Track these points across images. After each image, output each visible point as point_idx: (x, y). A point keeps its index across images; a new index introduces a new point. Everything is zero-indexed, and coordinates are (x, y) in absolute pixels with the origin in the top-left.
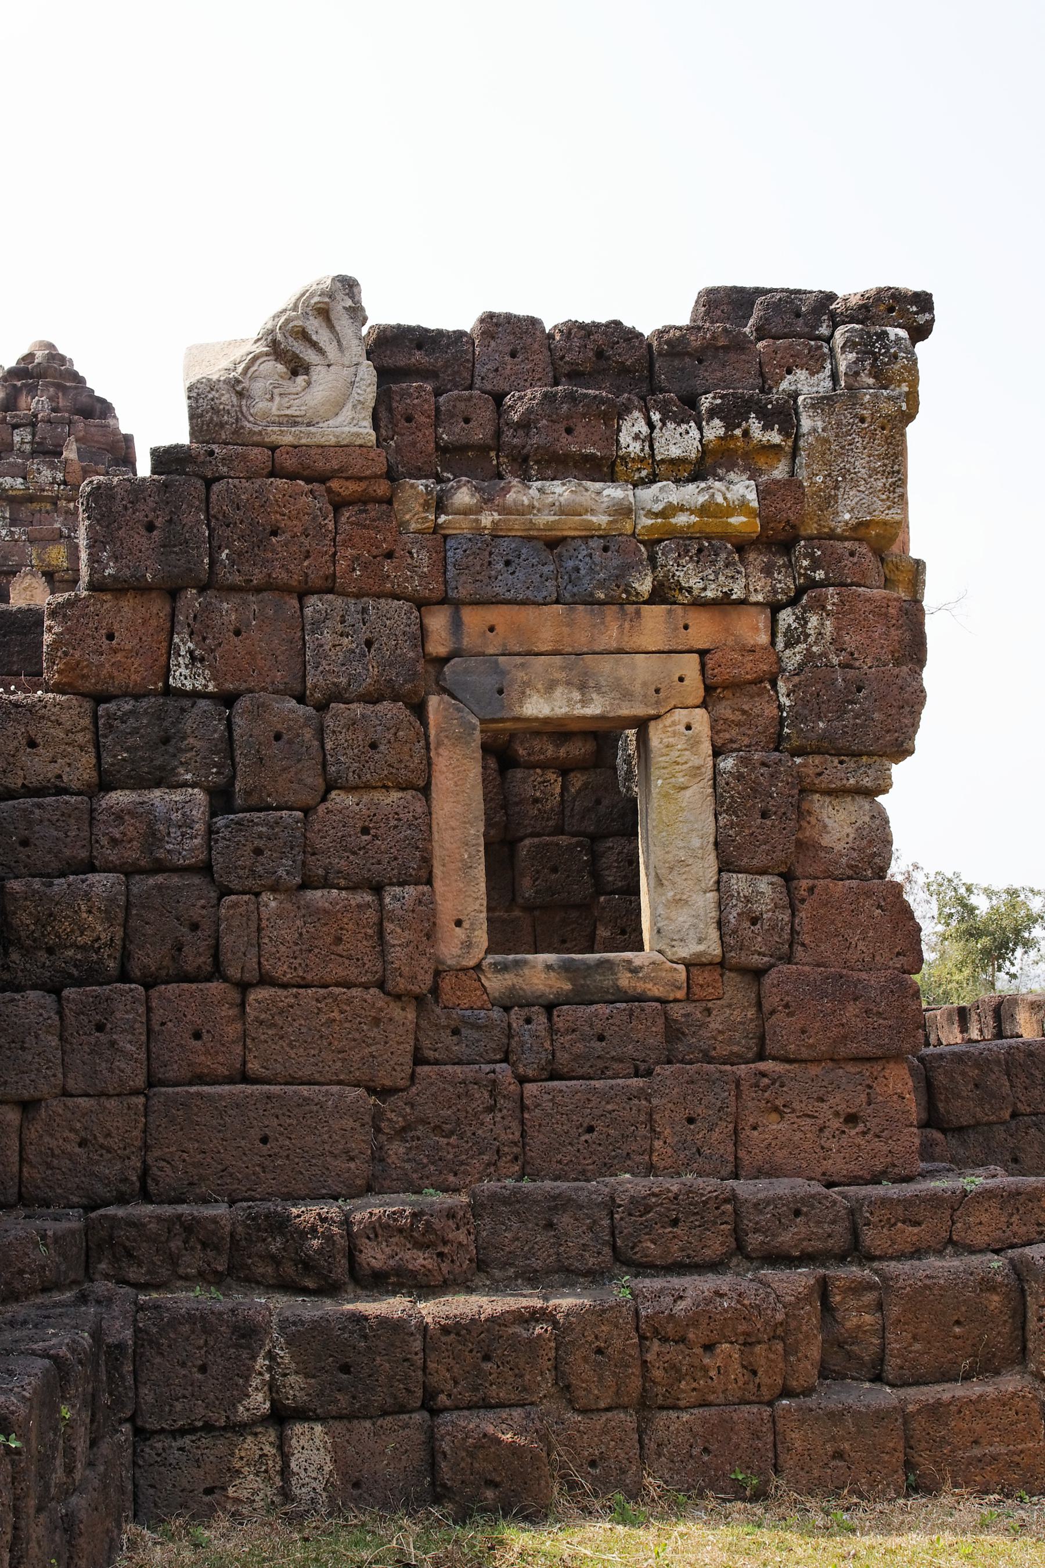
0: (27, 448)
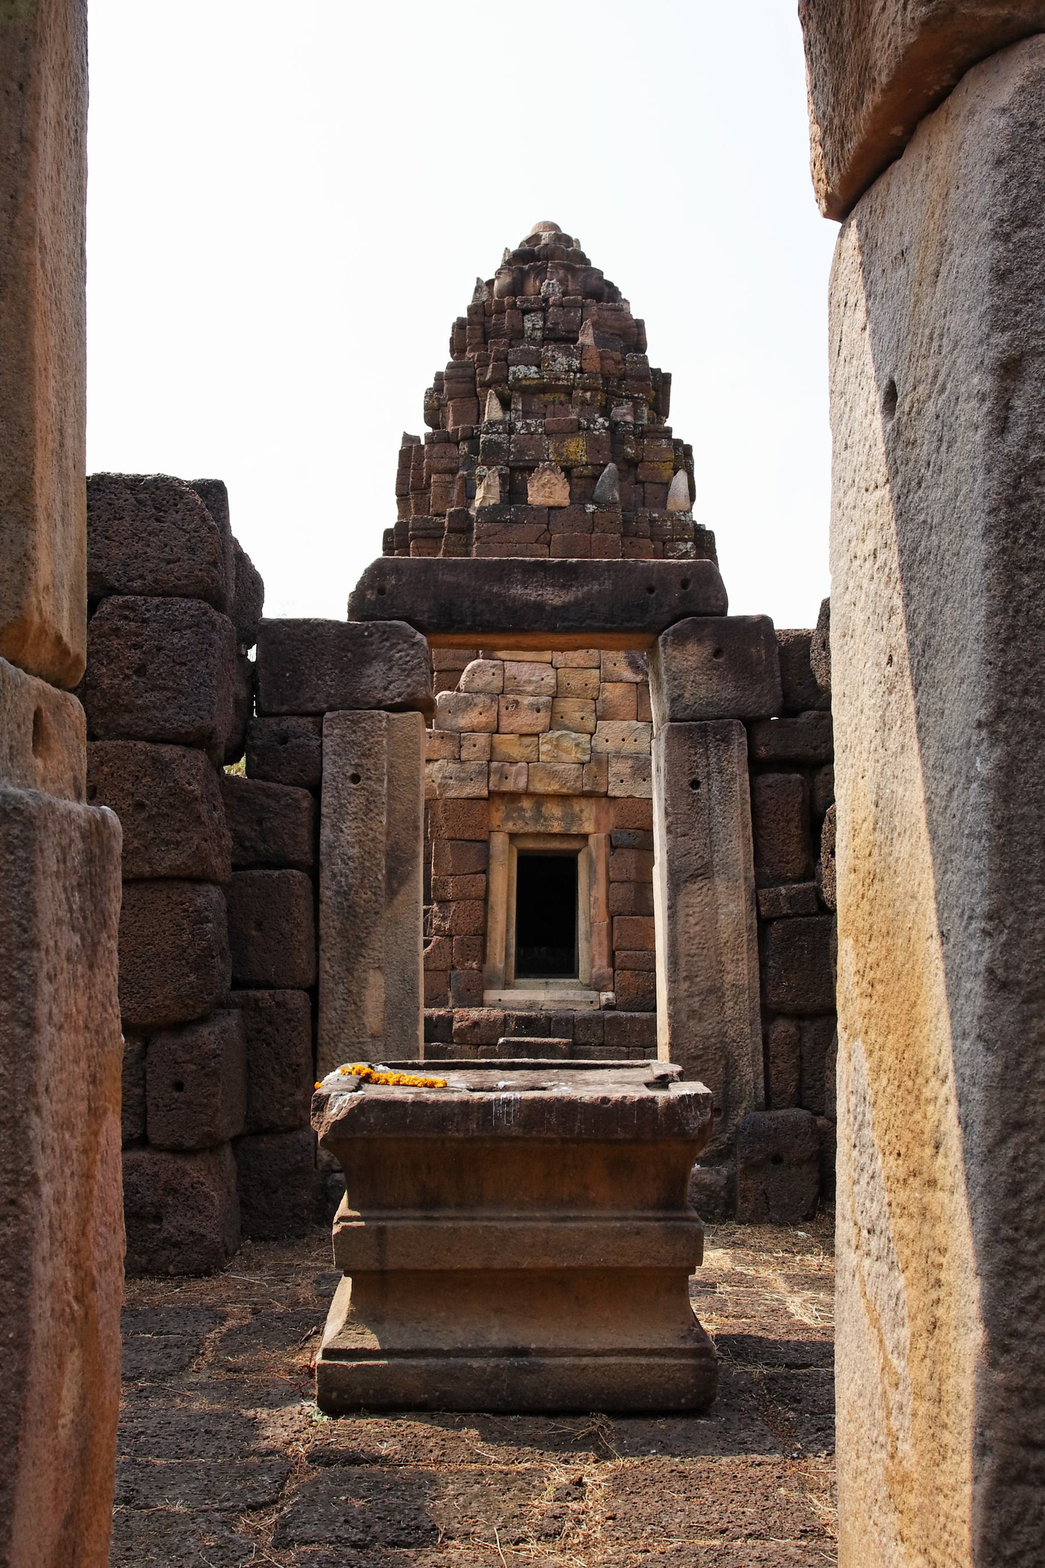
0: (539, 334)
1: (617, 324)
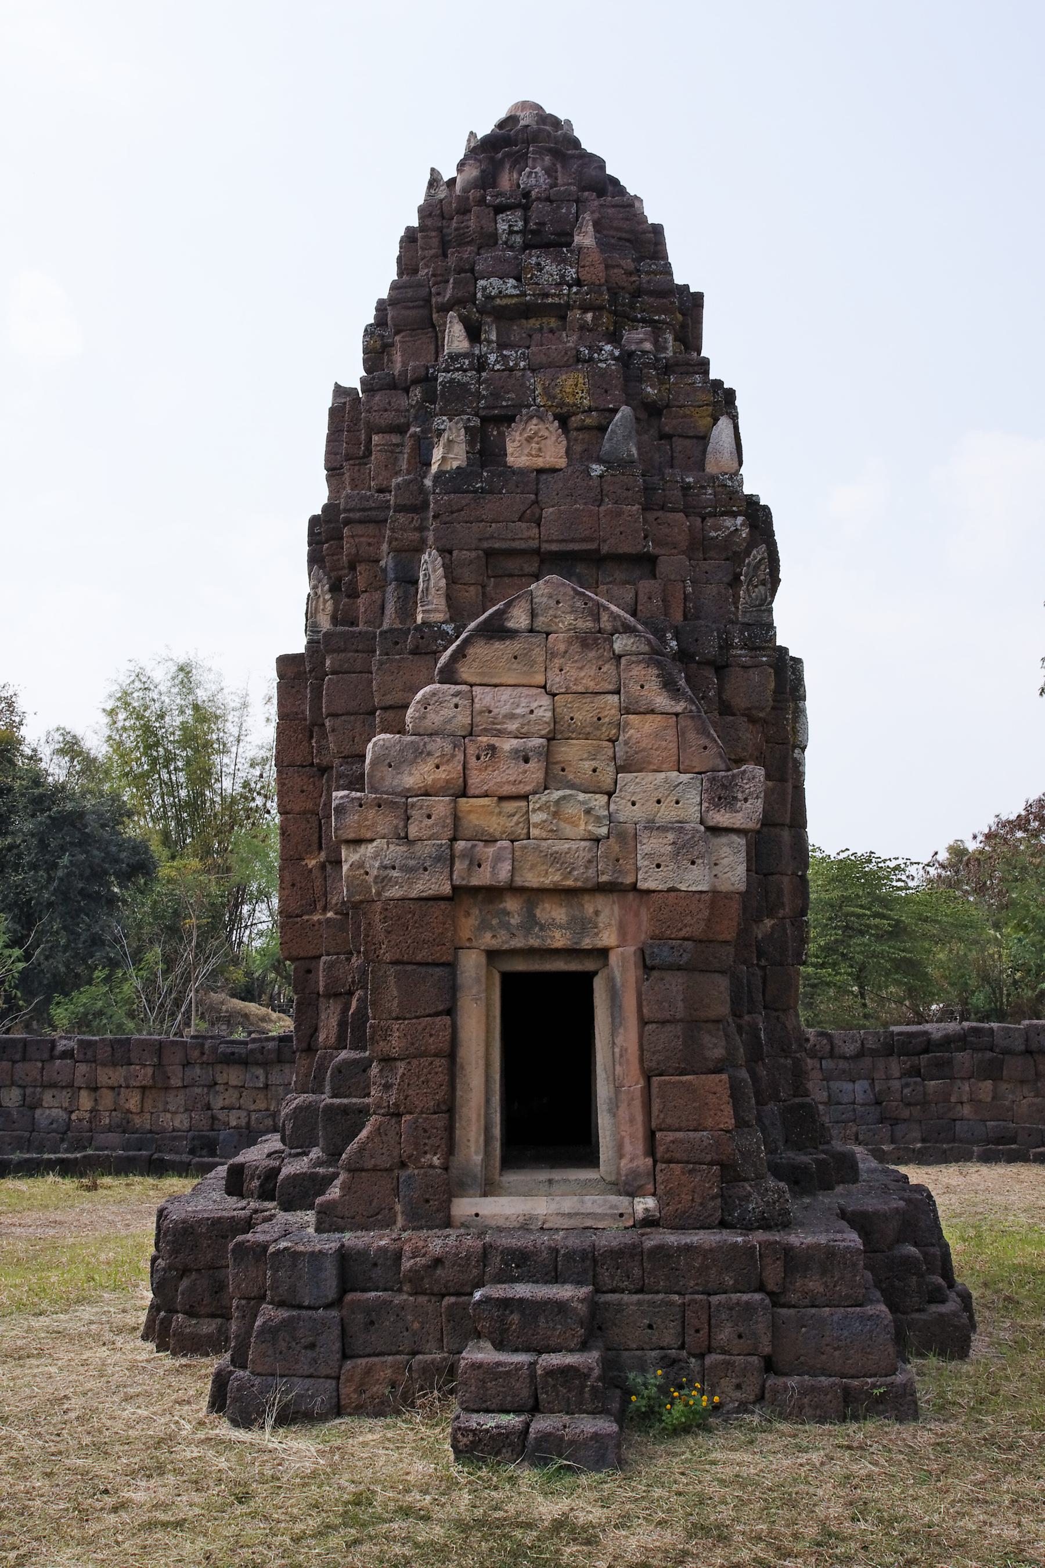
0: (518, 239)
1: (625, 225)
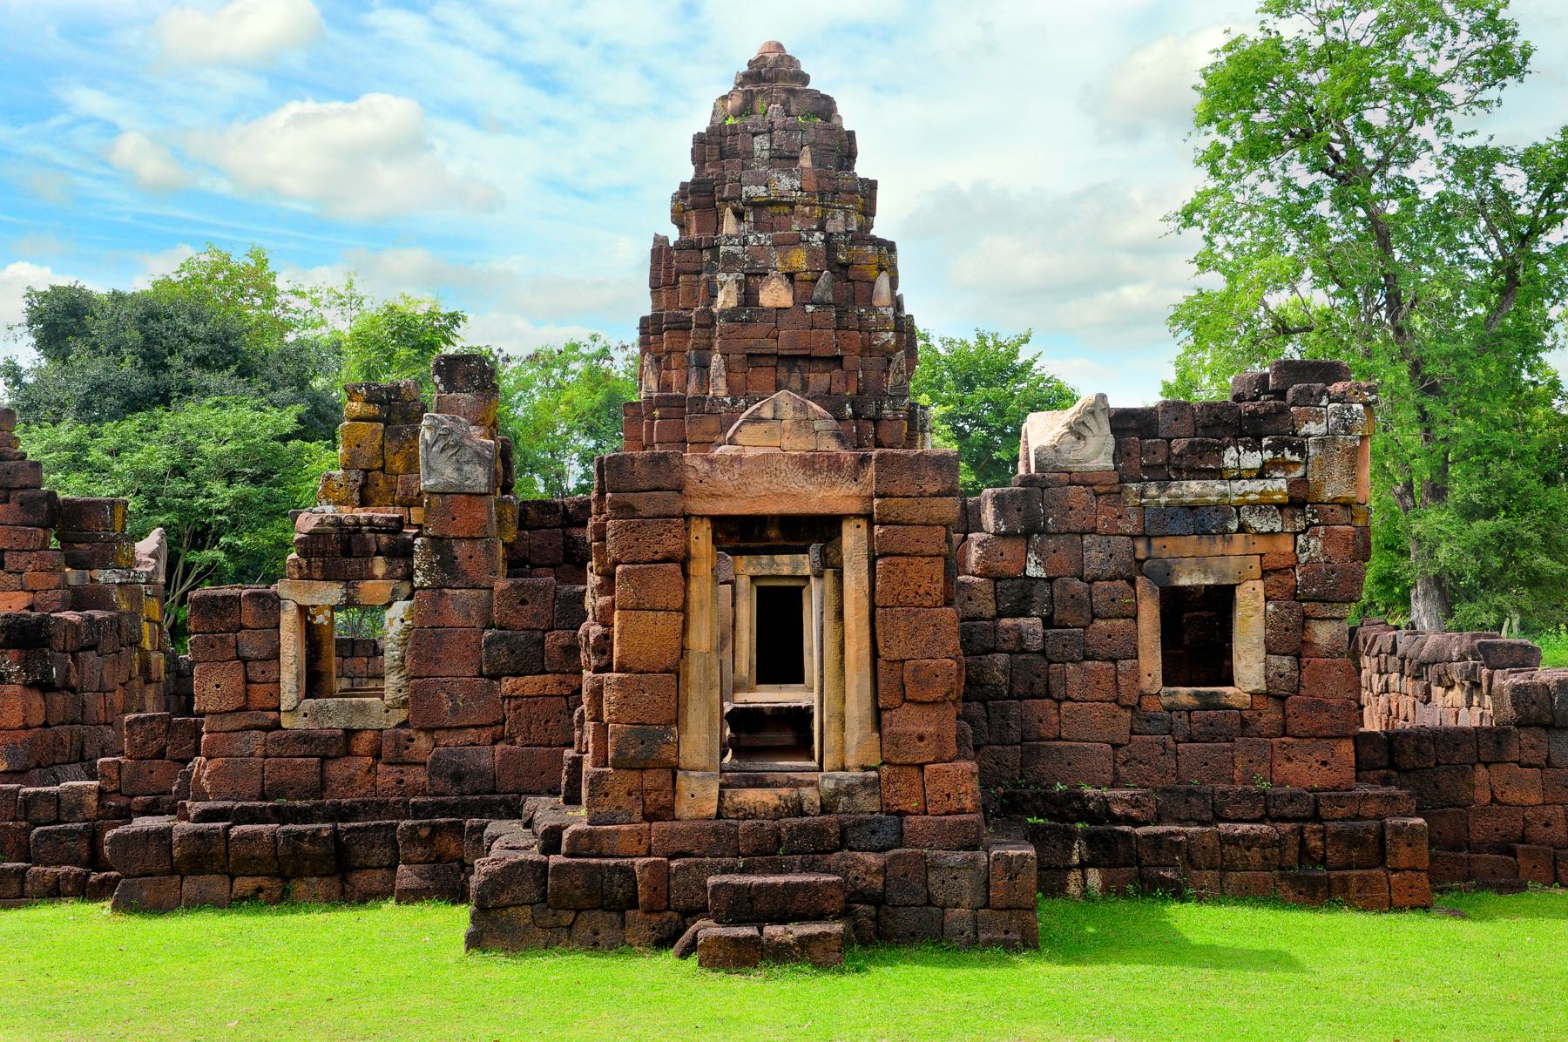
0: (766, 154)
